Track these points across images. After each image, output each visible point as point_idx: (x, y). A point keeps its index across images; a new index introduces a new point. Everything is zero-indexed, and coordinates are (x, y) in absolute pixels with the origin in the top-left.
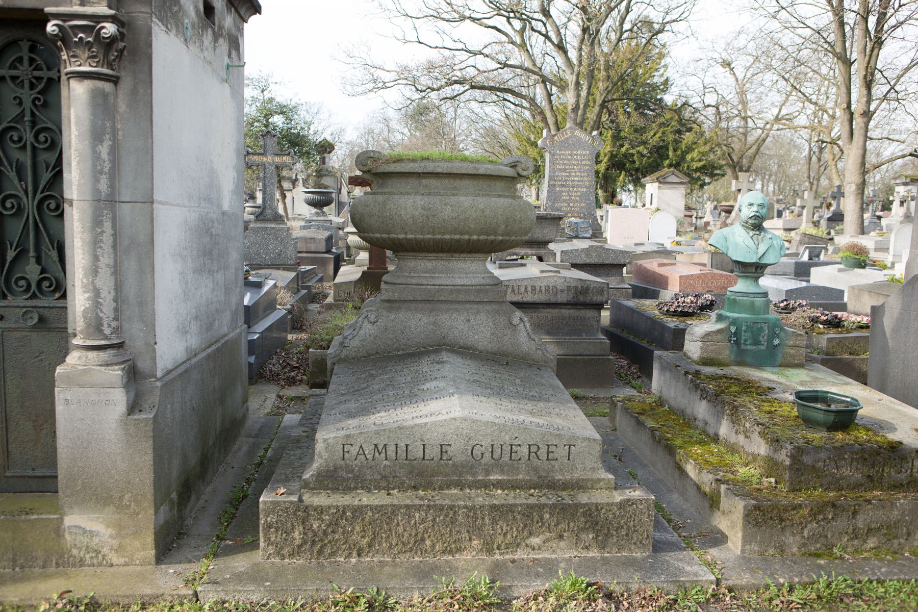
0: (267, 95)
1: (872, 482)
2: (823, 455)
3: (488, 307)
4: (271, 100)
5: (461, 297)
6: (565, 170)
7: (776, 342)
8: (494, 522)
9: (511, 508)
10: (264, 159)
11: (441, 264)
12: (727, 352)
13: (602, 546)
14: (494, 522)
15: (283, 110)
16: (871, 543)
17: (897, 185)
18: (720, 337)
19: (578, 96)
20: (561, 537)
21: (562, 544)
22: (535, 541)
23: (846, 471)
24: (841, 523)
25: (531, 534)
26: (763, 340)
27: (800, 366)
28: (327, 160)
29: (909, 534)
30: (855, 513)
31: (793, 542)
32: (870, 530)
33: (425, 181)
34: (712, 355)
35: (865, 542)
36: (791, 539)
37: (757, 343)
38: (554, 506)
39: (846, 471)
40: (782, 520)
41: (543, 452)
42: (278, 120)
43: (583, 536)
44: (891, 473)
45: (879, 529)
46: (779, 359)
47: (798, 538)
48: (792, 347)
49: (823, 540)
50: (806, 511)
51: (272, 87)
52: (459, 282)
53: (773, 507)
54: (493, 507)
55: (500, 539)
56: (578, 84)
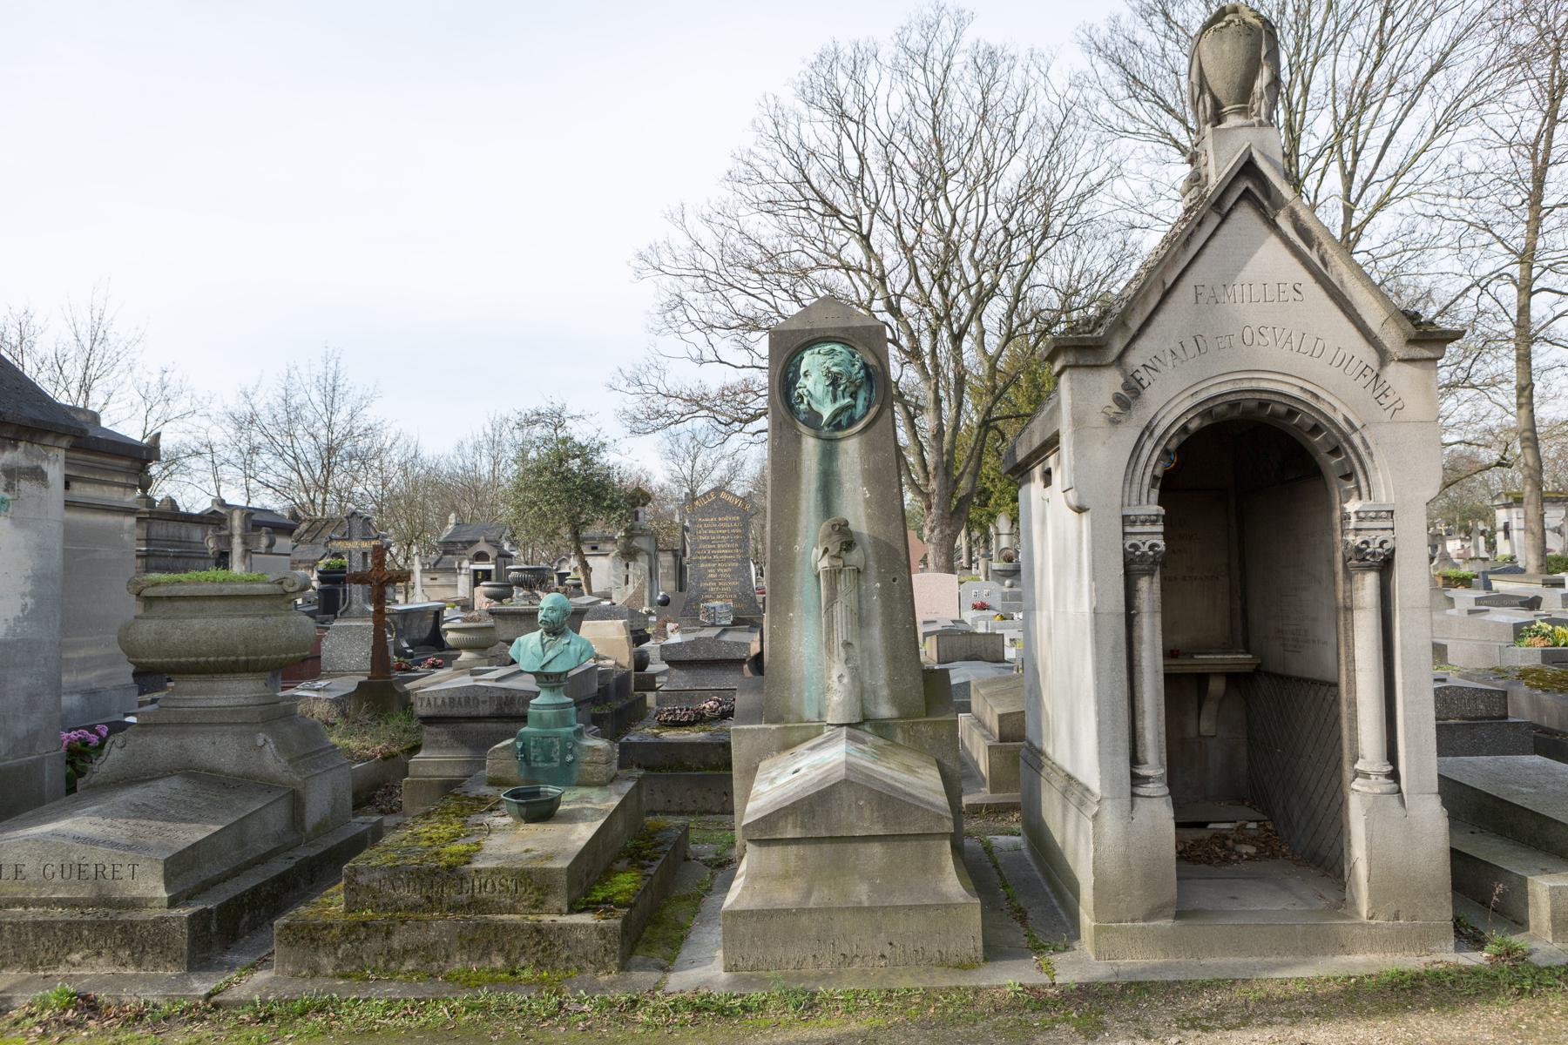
0: (561, 434)
1: (431, 903)
2: (377, 875)
3: (237, 729)
4: (564, 441)
5: (216, 719)
6: (710, 541)
7: (569, 758)
8: (37, 938)
9: (52, 925)
10: (349, 545)
11: (205, 685)
12: (516, 771)
13: (139, 964)
14: (37, 938)
15: (583, 452)
16: (409, 965)
17: (1498, 507)
18: (505, 754)
19: (940, 418)
20: (99, 954)
21: (101, 961)
22: (76, 957)
23: (403, 892)
24: (375, 944)
25: (71, 951)
26: (556, 756)
27: (601, 785)
28: (641, 515)
29: (448, 957)
30: (389, 934)
31: (327, 962)
32: (406, 952)
33: (177, 604)
34: (500, 774)
35: (402, 964)
36: (325, 960)
37: (550, 760)
38: (92, 923)
39: (403, 892)
40: (312, 939)
41: (109, 870)
42: (575, 464)
43: (121, 953)
44: (451, 894)
45: (415, 951)
46: (576, 777)
47: (332, 959)
48: (589, 763)
49: (358, 961)
50: (336, 931)
51: (568, 423)
52: (214, 703)
53: (304, 926)
54: (36, 924)
55: (43, 954)
56: (938, 401)
